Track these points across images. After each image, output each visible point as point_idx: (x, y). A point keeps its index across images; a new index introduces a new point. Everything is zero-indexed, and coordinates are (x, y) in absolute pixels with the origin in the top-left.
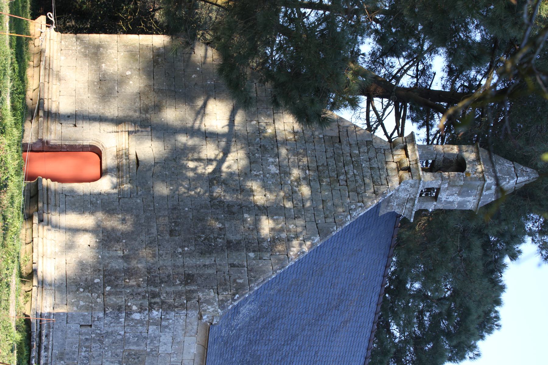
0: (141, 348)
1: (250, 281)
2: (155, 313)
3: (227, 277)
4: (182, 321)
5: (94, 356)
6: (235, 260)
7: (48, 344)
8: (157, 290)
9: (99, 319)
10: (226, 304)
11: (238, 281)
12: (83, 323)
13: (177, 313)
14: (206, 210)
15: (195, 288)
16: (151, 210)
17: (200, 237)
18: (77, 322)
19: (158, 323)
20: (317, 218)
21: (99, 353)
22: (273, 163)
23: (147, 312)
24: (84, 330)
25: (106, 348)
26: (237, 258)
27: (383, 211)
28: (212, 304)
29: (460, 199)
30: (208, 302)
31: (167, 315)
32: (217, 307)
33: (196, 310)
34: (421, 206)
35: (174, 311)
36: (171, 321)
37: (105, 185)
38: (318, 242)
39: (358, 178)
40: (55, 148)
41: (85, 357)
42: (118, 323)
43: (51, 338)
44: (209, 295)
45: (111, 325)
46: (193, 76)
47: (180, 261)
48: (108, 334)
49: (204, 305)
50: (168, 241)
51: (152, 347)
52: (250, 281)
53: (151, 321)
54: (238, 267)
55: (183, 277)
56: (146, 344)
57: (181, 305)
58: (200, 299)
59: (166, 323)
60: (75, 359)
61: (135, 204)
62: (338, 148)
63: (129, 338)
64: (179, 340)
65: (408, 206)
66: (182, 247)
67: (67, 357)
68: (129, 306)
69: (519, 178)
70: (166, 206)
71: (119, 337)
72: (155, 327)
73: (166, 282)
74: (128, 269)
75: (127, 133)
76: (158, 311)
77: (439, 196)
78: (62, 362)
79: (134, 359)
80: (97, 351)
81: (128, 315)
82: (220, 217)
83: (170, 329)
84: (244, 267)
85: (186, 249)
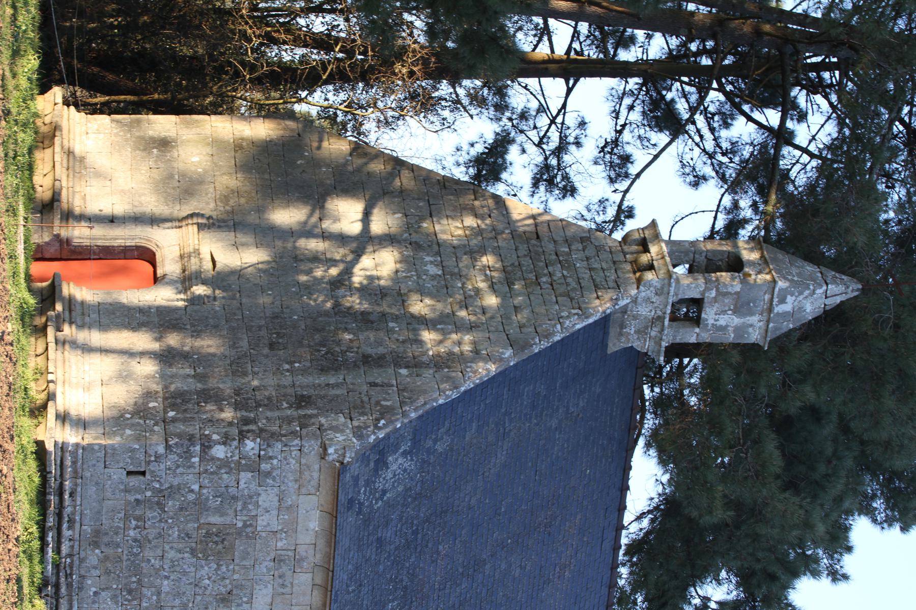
0: (228, 520)
1: (402, 403)
2: (249, 444)
3: (366, 399)
4: (294, 462)
5: (150, 537)
6: (377, 378)
7: (73, 513)
8: (252, 415)
9: (158, 458)
10: (365, 432)
11: (383, 403)
12: (131, 468)
13: (286, 445)
14: (327, 319)
15: (315, 412)
16: (238, 319)
17: (319, 351)
18: (121, 465)
19: (254, 466)
20: (506, 328)
21: (158, 531)
22: (431, 262)
23: (235, 443)
24: (134, 481)
25: (170, 521)
26: (377, 375)
27: (614, 345)
28: (342, 431)
29: (736, 321)
30: (336, 429)
31: (269, 450)
32: (351, 435)
33: (317, 439)
34: (675, 337)
35: (281, 441)
36: (275, 462)
37: (164, 296)
38: (510, 357)
39: (569, 280)
40: (80, 253)
41: (135, 540)
42: (189, 467)
43: (79, 499)
44: (338, 420)
45: (178, 471)
46: (299, 162)
47: (287, 380)
48: (174, 491)
49: (329, 432)
50: (267, 356)
51: (245, 518)
52: (402, 403)
53: (243, 462)
54: (382, 386)
55: (293, 400)
56: (236, 511)
57: (291, 433)
58: (321, 425)
59: (268, 466)
60: (118, 546)
61: (212, 312)
62: (534, 245)
63: (207, 499)
64: (290, 503)
65: (653, 334)
66: (291, 363)
67: (106, 539)
68: (206, 435)
69: (830, 286)
70: (262, 314)
71: (191, 497)
72: (250, 475)
73: (265, 405)
74: (204, 390)
75: (195, 227)
76: (254, 440)
77: (703, 315)
78: (97, 551)
79: (216, 543)
80: (154, 528)
81: (206, 446)
82: (350, 326)
83: (274, 479)
84: (393, 386)
85: (297, 365)
